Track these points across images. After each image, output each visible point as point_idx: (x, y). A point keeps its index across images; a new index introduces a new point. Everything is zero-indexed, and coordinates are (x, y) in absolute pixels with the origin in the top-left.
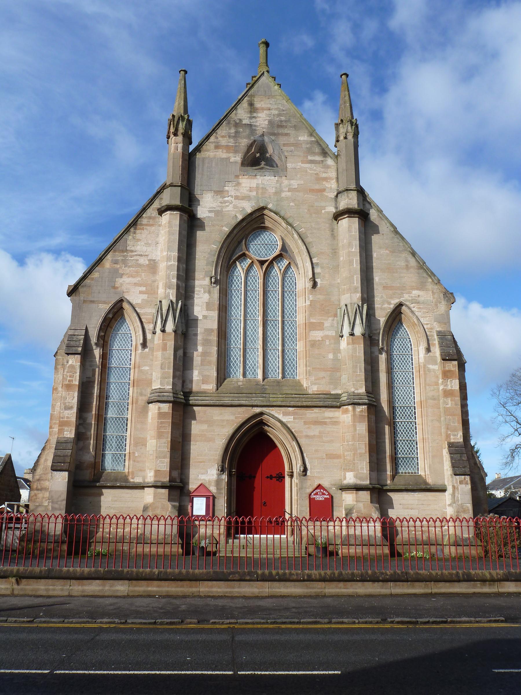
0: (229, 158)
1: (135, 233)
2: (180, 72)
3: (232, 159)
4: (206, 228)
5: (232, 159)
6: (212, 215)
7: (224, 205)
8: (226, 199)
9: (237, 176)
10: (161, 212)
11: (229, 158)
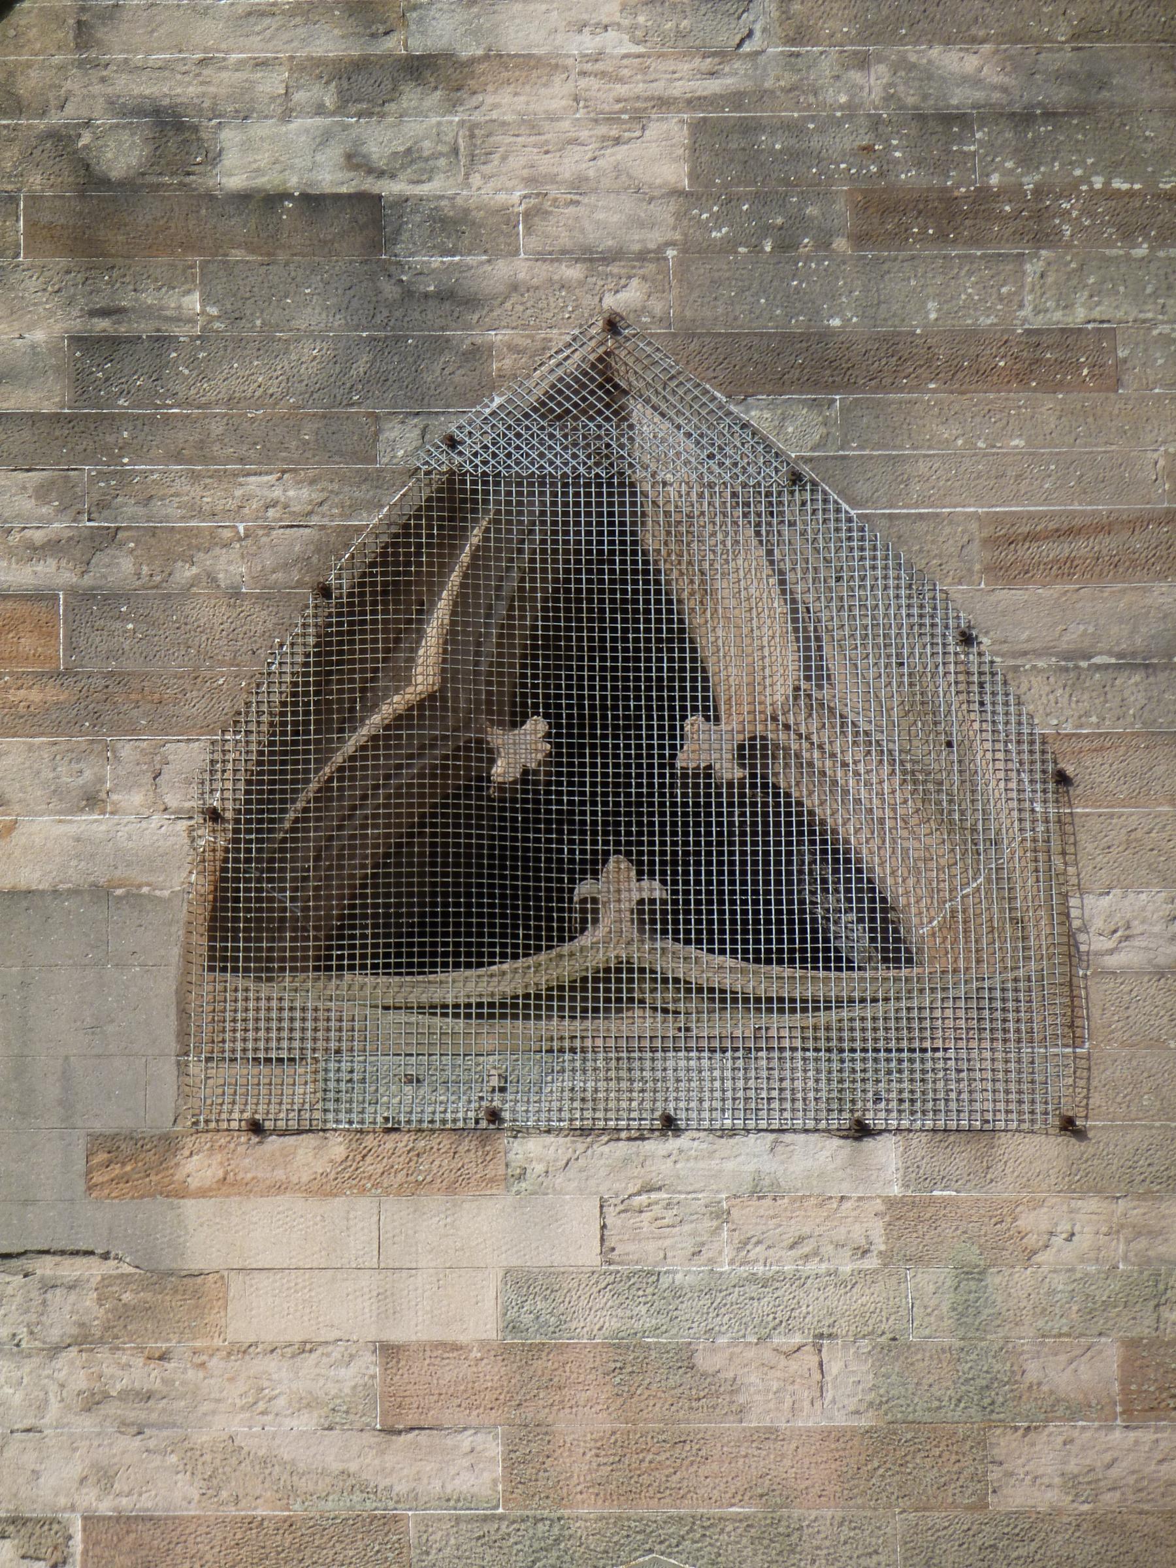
9: (133, 1159)
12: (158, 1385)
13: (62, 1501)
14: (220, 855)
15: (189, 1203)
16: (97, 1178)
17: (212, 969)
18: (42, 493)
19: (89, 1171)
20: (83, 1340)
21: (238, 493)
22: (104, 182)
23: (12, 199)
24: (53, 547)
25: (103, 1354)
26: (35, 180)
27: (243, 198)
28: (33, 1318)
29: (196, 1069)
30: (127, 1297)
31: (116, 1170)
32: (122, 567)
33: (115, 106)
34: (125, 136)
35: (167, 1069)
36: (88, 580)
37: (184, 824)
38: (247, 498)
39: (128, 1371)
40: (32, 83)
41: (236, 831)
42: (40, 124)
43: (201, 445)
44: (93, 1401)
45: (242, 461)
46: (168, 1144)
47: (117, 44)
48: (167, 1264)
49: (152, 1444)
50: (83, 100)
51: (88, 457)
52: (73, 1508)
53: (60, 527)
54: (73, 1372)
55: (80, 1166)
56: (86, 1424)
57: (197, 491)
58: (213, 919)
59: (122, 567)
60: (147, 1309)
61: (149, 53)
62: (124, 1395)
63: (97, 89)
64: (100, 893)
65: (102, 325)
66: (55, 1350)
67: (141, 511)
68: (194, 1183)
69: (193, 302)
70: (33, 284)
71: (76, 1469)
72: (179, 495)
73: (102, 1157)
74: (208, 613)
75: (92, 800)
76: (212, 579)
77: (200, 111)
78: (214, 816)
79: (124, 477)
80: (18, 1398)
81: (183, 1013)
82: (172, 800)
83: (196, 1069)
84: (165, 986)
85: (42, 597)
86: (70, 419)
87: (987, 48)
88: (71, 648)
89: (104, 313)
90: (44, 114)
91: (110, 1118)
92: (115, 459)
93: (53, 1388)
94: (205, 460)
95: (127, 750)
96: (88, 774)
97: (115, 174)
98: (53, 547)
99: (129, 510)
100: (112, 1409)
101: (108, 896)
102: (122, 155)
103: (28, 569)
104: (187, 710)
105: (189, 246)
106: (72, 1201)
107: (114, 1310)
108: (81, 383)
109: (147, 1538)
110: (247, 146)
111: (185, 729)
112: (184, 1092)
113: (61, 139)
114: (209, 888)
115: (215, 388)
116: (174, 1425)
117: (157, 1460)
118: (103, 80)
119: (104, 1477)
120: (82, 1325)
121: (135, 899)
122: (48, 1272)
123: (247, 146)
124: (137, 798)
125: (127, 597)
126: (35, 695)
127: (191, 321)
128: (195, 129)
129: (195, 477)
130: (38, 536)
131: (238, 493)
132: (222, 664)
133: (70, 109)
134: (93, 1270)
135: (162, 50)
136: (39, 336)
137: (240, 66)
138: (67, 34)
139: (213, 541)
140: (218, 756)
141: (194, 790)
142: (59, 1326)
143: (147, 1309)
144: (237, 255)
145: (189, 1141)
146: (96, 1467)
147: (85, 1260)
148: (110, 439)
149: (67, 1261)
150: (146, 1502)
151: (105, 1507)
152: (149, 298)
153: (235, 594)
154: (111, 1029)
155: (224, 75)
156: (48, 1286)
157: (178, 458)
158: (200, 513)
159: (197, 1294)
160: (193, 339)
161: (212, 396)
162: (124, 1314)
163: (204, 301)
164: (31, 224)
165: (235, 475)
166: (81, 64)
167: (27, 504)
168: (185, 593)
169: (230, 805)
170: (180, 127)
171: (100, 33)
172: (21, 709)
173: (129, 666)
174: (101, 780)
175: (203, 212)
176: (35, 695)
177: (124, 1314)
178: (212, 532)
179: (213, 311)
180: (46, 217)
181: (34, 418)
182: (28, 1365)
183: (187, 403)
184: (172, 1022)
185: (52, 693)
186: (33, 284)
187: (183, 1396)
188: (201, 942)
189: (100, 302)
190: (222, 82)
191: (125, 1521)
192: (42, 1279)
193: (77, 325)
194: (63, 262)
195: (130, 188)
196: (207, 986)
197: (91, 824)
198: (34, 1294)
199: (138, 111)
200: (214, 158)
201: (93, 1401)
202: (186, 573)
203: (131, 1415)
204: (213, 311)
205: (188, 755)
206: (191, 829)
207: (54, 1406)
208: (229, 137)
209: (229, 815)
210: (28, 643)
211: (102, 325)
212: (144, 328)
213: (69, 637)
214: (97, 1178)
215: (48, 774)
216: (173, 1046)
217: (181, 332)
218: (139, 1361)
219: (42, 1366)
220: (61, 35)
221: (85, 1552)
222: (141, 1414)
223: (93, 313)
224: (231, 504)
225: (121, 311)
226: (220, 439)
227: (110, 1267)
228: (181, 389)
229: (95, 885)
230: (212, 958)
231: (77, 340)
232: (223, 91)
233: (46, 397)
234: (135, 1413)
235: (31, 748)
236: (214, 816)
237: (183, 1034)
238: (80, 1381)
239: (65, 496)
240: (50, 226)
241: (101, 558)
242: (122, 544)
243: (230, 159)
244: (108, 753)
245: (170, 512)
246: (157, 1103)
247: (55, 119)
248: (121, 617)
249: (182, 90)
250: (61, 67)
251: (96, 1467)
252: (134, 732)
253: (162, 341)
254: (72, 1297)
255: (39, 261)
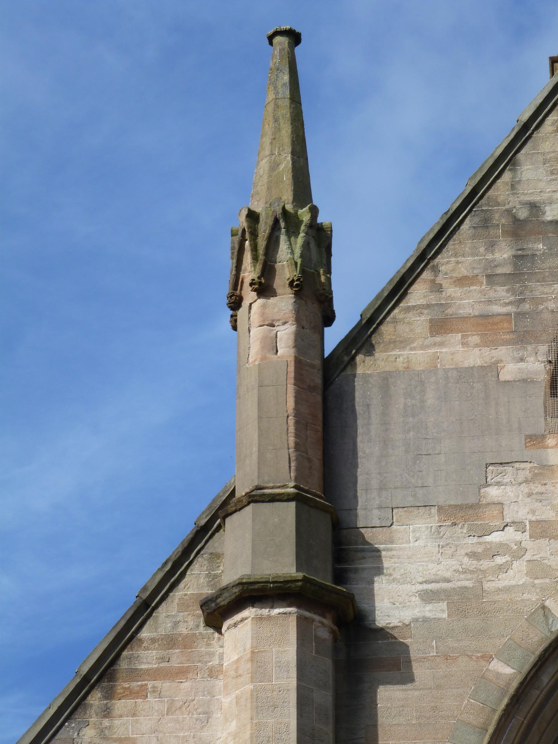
0: (494, 368)
1: (107, 713)
2: (271, 38)
3: (510, 371)
4: (418, 670)
5: (510, 371)
6: (438, 611)
7: (485, 564)
8: (495, 537)
9: (536, 440)
10: (217, 612)
11: (494, 368)
12: (544, 491)
13: (524, 518)
14: (552, 371)
15: (549, 450)
16: (528, 445)
17: (551, 397)
18: (508, 291)
19: (526, 443)
20: (526, 481)
21: (552, 288)
22: (519, 220)
23: (498, 225)
24: (510, 303)
25: (531, 484)
26: (503, 221)
27: (551, 222)
28: (515, 477)
29: (549, 419)
30: (536, 471)
31: (532, 443)
32: (526, 307)
33: (521, 203)
34: (523, 209)
35: (542, 420)
36: (519, 310)
37: (543, 364)
38: (555, 289)
39: (537, 488)
40: (501, 199)
41: (555, 365)
42: (504, 208)
43: (543, 278)
44: (530, 495)
45: (553, 281)
46: (543, 437)
47: (521, 189)
48: (545, 463)
49: (544, 504)
50: (514, 202)
51: (518, 282)
52: (526, 519)
53: (512, 298)
54: (524, 488)
55: (524, 442)
56: (528, 500)
57: (543, 288)
58: (551, 385)
59: (526, 307)
60: (541, 474)
61: (528, 190)
62: (537, 493)
63: (516, 199)
64: (524, 381)
65: (520, 252)
66: (520, 484)
67: (530, 294)
68: (550, 445)
69: (541, 246)
70: (504, 244)
71: (527, 510)
72: (539, 289)
73: (529, 440)
74: (547, 316)
75: (522, 360)
76: (547, 308)
77: (540, 203)
78: (550, 362)
79: (526, 287)
80: (512, 495)
81: (545, 407)
82: (540, 359)
83: (549, 419)
84: (541, 401)
85: (508, 314)
86: (513, 274)
87: (115, 736)
88: (515, 326)
89: (520, 250)
90: (504, 206)
91: (529, 432)
92: (524, 283)
93: (520, 492)
94: (544, 281)
95: (529, 348)
96: (521, 354)
97: (521, 218)
98: (510, 303)
99: (528, 294)
100: (534, 496)
101: (526, 381)
102: (523, 214)
103: (505, 308)
104: (543, 338)
105: (539, 233)
106: (522, 450)
107: (533, 474)
108: (515, 266)
109: (544, 525)
110: (552, 210)
111: (543, 342)
112: (546, 425)
113: (509, 211)
114: (550, 378)
115: (547, 265)
116: (548, 500)
117: (545, 508)
118: (518, 197)
119: (533, 512)
120: (526, 478)
121: (533, 381)
122: (518, 466)
123: (552, 210)
124: (532, 359)
125: (528, 313)
126: (508, 337)
127: (540, 250)
128: (539, 207)
129: (542, 285)
130: (507, 301)
131: (552, 288)
132: (550, 327)
133: (510, 204)
134: (528, 465)
135: (531, 190)
136: (505, 256)
137: (549, 192)
138: (509, 187)
139: (547, 300)
140: (550, 348)
141: (545, 356)
142: (521, 478)
143: (541, 474)
144: (550, 235)
145: (548, 436)
146: (531, 509)
147: (526, 463)
148: (522, 278)
149: (522, 464)
150: (543, 517)
151: (534, 519)
152: (530, 246)
153: (553, 311)
154: (529, 411)
155: (546, 194)
156: (518, 469)
157: (538, 281)
158: (544, 294)
159: (552, 470)
160: (541, 254)
161: (545, 267)
162: (536, 475)
163: (543, 245)
164: (503, 231)
165: (552, 284)
166: (513, 194)
167: (504, 294)
168: (541, 312)
169: (553, 359)
170: (536, 207)
171: (517, 186)
172: (505, 340)
173: (529, 329)
174: (524, 355)
175: (370, 386)
176: (508, 337)
177: (536, 475)
178: (547, 298)
179: (545, 248)
180: (506, 229)
181: (505, 274)
182: (514, 487)
183: (540, 269)
184: (543, 409)
185: (512, 336)
186: (504, 244)
187: (550, 493)
188: (548, 391)
189: (519, 247)
190: (545, 196)
191: (538, 522)
192: (516, 468)
193: (513, 252)
194: (510, 239)
195: (525, 221)
196: (550, 401)
197: (522, 365)
198: (515, 471)
199: (526, 204)
200: (544, 213)
201: (530, 495)
202: (541, 307)
203: (538, 498)
204: (545, 248)
205: (543, 348)
206: (545, 365)
207: (521, 496)
208: (547, 208)
209: (553, 362)
210: (506, 325)
211: (520, 252)
212: (529, 253)
213: (515, 323)
214: (528, 445)
215: (511, 354)
216: (543, 414)
217: (538, 253)
218: (540, 486)
219: (517, 487)
220: (507, 187)
221: (530, 529)
222: (541, 497)
223: (518, 250)
224: (551, 291)
225: (524, 249)
226: (548, 277)
227: (532, 465)
228: (538, 266)
229: (523, 379)
230: (551, 394)
231: (514, 256)
232: (546, 198)
233: (507, 269)
234: (539, 497)
235: (507, 349)
236: (550, 362)
237: (545, 412)
238: (526, 490)
239: (513, 292)
240: (507, 231)
241: (521, 305)
242: (526, 302)
243: (548, 213)
244: (525, 349)
245: (537, 294)
246: (540, 427)
247: (507, 207)
248: (527, 318)
249: (536, 198)
250: (508, 195)
251: (531, 509)
252: (530, 344)
253: (534, 255)
254: (523, 472)
255: (505, 239)
